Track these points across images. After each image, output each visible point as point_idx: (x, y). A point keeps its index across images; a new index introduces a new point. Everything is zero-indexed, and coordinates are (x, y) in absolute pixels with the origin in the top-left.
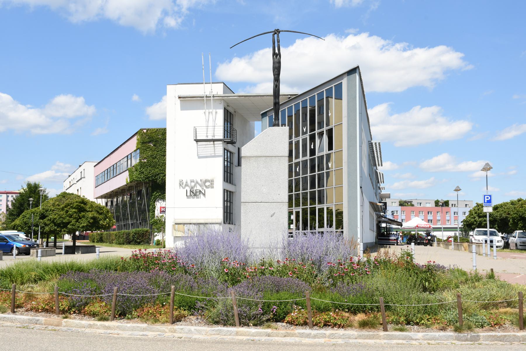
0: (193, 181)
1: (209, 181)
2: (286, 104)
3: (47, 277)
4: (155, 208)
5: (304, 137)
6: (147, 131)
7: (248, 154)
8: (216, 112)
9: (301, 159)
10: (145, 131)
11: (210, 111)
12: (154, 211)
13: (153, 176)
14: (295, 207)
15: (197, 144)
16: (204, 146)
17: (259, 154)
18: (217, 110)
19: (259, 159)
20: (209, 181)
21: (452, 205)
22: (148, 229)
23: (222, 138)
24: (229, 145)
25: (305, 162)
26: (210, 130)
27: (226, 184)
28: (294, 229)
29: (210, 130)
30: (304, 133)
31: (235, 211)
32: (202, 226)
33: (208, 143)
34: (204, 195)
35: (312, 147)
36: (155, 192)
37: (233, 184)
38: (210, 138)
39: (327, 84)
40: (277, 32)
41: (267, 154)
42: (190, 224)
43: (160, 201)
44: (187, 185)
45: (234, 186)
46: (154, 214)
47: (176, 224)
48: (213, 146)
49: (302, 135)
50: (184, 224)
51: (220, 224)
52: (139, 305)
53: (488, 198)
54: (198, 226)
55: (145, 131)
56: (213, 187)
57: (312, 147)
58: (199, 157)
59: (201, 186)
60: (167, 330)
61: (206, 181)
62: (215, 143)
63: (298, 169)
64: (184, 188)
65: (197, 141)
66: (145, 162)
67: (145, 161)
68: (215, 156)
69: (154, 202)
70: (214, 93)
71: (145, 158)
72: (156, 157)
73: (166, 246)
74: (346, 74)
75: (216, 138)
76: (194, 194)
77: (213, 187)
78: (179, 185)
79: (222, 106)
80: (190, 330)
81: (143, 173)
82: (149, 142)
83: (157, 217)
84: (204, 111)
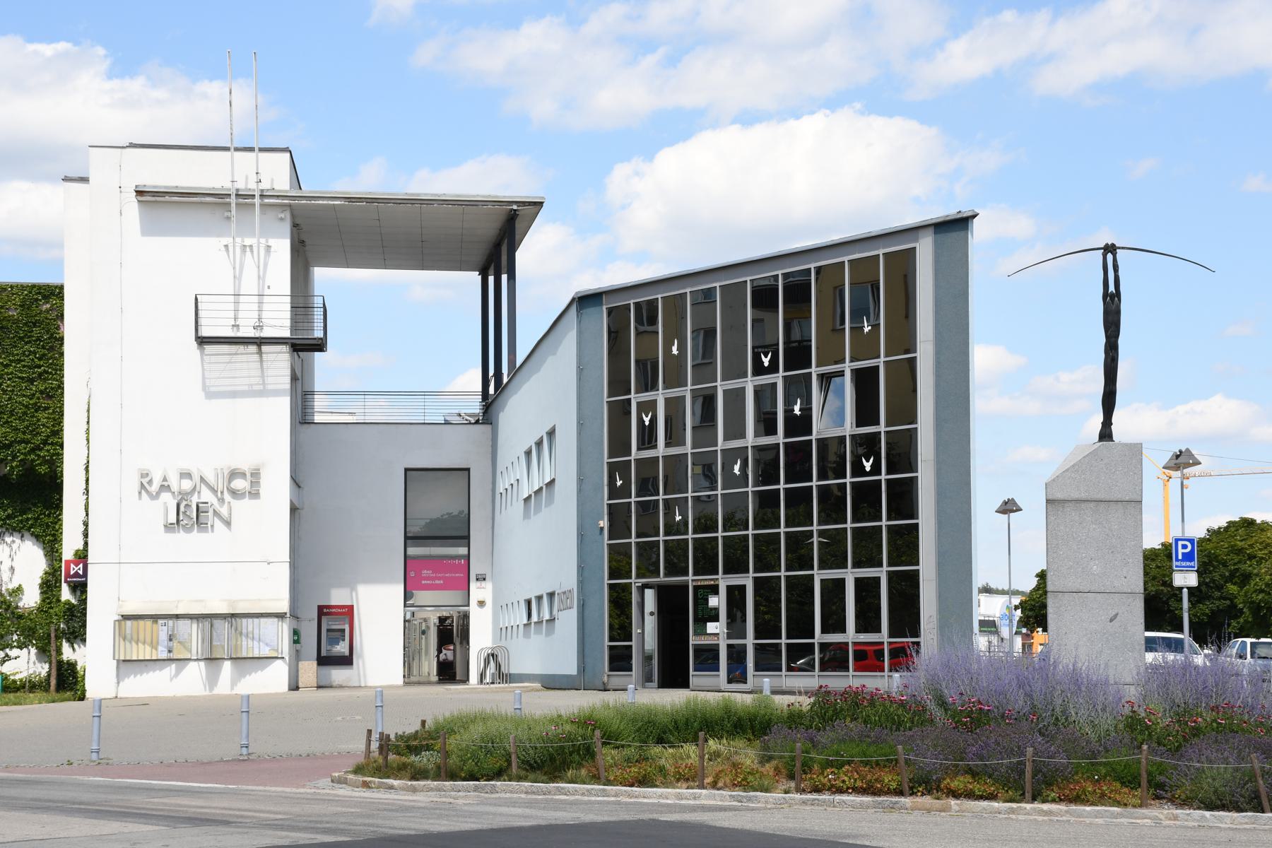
0: (186, 475)
1: (243, 475)
3: (607, 755)
14: (725, 572)
16: (226, 358)
17: (1083, 496)
18: (272, 242)
19: (1083, 505)
20: (243, 475)
23: (287, 334)
28: (723, 636)
32: (222, 627)
33: (241, 348)
34: (228, 523)
35: (797, 411)
39: (858, 245)
40: (1110, 249)
41: (1101, 496)
42: (177, 617)
43: (8, 539)
47: (126, 618)
48: (256, 357)
50: (155, 618)
51: (280, 616)
53: (1184, 547)
56: (255, 495)
57: (797, 411)
58: (210, 395)
59: (214, 491)
60: (1161, 816)
61: (234, 474)
62: (264, 348)
65: (202, 341)
68: (263, 393)
73: (88, 695)
74: (931, 230)
75: (267, 333)
76: (191, 517)
77: (255, 495)
78: (137, 487)
80: (1203, 817)
84: (225, 240)
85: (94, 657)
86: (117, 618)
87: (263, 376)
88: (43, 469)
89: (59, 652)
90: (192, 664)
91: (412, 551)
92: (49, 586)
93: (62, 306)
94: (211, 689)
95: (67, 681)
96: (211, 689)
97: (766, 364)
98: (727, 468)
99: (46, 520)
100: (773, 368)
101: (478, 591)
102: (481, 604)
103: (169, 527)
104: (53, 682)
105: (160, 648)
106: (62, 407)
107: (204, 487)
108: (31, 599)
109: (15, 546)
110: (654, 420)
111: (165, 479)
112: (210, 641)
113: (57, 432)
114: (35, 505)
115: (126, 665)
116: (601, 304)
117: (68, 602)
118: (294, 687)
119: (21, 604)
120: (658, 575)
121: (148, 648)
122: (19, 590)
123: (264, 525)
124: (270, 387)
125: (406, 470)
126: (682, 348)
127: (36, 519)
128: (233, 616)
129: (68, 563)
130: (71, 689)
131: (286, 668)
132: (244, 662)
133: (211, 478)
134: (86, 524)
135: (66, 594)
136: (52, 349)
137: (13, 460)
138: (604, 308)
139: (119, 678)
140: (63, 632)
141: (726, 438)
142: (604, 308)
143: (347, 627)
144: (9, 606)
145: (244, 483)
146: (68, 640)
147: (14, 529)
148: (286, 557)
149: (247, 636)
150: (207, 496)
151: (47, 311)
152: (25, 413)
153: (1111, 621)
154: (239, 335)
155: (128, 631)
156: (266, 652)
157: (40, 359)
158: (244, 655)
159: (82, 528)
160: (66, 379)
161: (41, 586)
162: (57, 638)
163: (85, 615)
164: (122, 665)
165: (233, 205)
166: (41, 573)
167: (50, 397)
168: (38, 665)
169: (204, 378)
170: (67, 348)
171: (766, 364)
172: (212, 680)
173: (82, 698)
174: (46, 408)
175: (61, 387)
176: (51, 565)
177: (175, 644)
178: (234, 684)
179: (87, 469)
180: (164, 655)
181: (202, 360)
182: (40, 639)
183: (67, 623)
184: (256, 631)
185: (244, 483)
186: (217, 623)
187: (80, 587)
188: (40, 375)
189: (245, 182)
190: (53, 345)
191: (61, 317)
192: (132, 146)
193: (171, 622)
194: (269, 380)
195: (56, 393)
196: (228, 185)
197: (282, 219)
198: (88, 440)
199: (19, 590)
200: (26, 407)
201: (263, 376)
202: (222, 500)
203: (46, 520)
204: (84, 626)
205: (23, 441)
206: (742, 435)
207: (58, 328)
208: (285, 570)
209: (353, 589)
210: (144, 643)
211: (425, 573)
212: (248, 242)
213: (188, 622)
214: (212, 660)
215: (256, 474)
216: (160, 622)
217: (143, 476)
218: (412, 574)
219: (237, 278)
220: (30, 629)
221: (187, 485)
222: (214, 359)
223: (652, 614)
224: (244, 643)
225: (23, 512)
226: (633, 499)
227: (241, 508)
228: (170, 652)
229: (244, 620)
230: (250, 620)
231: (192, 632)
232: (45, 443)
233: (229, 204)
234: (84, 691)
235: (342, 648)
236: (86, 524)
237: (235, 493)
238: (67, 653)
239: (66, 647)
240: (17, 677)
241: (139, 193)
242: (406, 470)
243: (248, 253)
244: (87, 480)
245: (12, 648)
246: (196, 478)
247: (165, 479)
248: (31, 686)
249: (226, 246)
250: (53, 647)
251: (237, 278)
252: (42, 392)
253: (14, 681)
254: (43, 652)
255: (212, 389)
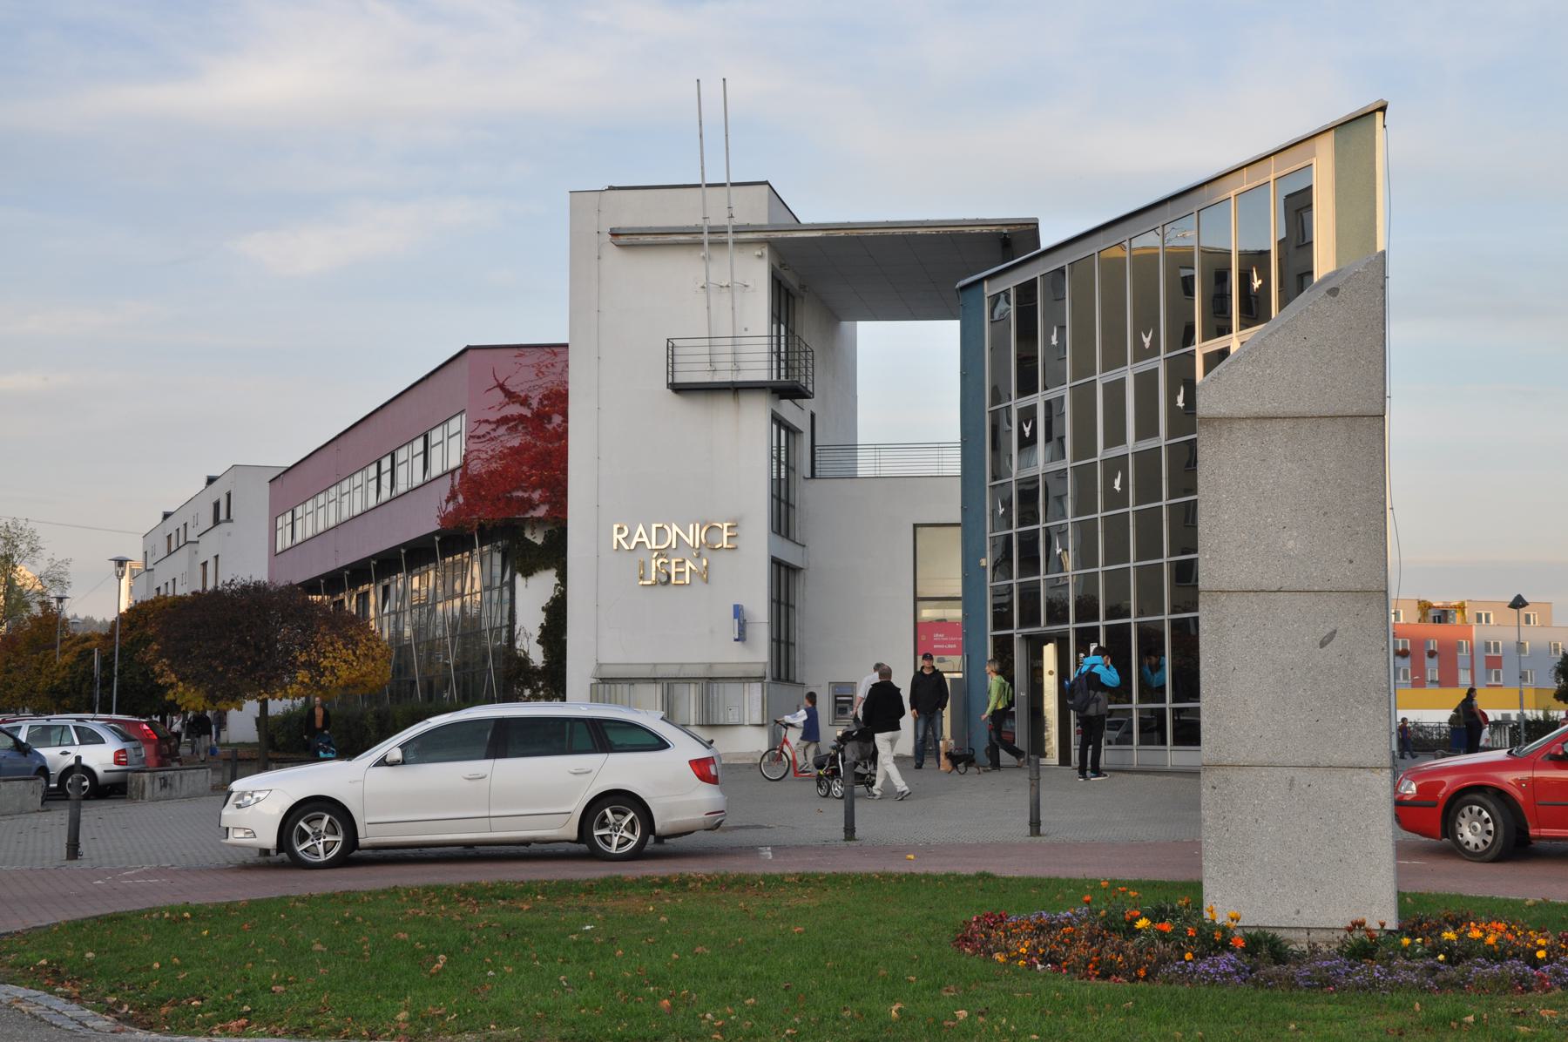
5: (1146, 366)
7: (1222, 409)
9: (1131, 445)
17: (1269, 408)
19: (1268, 424)
21: (1479, 617)
24: (786, 403)
25: (1148, 460)
27: (778, 539)
30: (1141, 354)
31: (798, 637)
37: (787, 536)
45: (800, 549)
47: (604, 680)
49: (1136, 360)
52: (83, 973)
63: (1117, 482)
65: (678, 389)
70: (740, 219)
97: (1147, 345)
98: (1108, 483)
100: (1154, 351)
110: (1034, 431)
120: (1038, 624)
125: (915, 526)
126: (1061, 337)
141: (1107, 446)
153: (1323, 644)
154: (716, 379)
171: (1147, 345)
189: (718, 218)
192: (611, 188)
196: (700, 222)
197: (760, 257)
206: (1123, 441)
211: (937, 636)
218: (923, 638)
223: (1051, 673)
242: (915, 526)
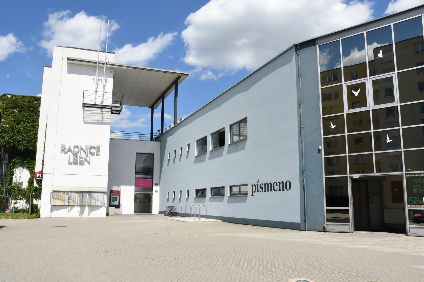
0: (77, 147)
1: (94, 148)
2: (365, 27)
4: (13, 174)
6: (12, 96)
8: (106, 80)
10: (9, 96)
11: (100, 78)
12: (12, 178)
13: (15, 142)
15: (84, 109)
16: (91, 112)
20: (94, 148)
22: (4, 196)
26: (100, 95)
29: (100, 95)
33: (96, 109)
36: (15, 159)
38: (98, 103)
42: (71, 192)
43: (19, 168)
44: (69, 150)
46: (11, 181)
47: (54, 191)
48: (101, 112)
50: (64, 192)
51: (105, 193)
54: (81, 195)
55: (9, 96)
56: (98, 155)
58: (85, 123)
59: (85, 152)
61: (92, 148)
62: (103, 110)
64: (65, 154)
66: (7, 127)
67: (7, 126)
68: (102, 123)
69: (13, 169)
71: (7, 123)
72: (20, 123)
73: (41, 216)
76: (77, 161)
77: (98, 155)
79: (112, 75)
81: (3, 137)
82: (14, 108)
83: (15, 183)
84: (93, 77)
85: (44, 204)
86: (52, 191)
87: (102, 118)
88: (31, 148)
89: (32, 201)
90: (76, 207)
91: (137, 176)
92: (30, 182)
93: (40, 102)
94: (81, 216)
95: (34, 211)
96: (81, 216)
99: (31, 163)
101: (155, 188)
102: (156, 191)
103: (70, 164)
104: (30, 211)
105: (65, 202)
106: (38, 131)
107: (82, 151)
108: (25, 185)
109: (21, 170)
111: (70, 148)
112: (82, 200)
113: (36, 138)
114: (28, 159)
115: (54, 207)
116: (316, 44)
117: (36, 187)
118: (108, 215)
119: (22, 187)
121: (61, 202)
122: (22, 183)
123: (101, 164)
124: (104, 122)
127: (28, 163)
128: (89, 192)
129: (37, 173)
130: (36, 213)
131: (106, 209)
132: (93, 208)
133: (84, 148)
134: (43, 161)
135: (35, 184)
136: (36, 114)
137: (22, 145)
138: (318, 46)
139: (52, 211)
140: (34, 195)
142: (318, 46)
143: (118, 197)
144: (18, 187)
145: (94, 150)
146: (35, 198)
147: (21, 165)
148: (106, 173)
149: (94, 199)
150: (83, 154)
151: (36, 104)
152: (27, 132)
155: (55, 196)
156: (100, 204)
157: (32, 117)
158: (93, 205)
159: (42, 162)
160: (39, 123)
161: (28, 182)
162: (32, 197)
163: (41, 190)
164: (53, 207)
165: (97, 67)
166: (28, 178)
167: (35, 128)
168: (26, 205)
169: (84, 118)
170: (41, 114)
172: (82, 213)
173: (39, 217)
174: (33, 131)
175: (38, 125)
176: (31, 176)
177: (70, 201)
178: (89, 214)
179: (44, 144)
180: (66, 204)
181: (84, 112)
182: (27, 197)
183: (35, 193)
184: (97, 198)
185: (94, 150)
186: (84, 194)
187: (40, 182)
188: (32, 121)
190: (37, 113)
191: (40, 106)
193: (69, 194)
194: (104, 120)
195: (36, 127)
197: (111, 72)
198: (45, 135)
199: (22, 183)
200: (27, 130)
201: (102, 118)
202: (87, 156)
203: (31, 163)
204: (41, 194)
205: (25, 140)
207: (39, 109)
208: (106, 178)
209: (119, 186)
210: (60, 200)
211: (140, 182)
212: (100, 78)
213: (75, 194)
214: (82, 206)
215: (99, 148)
216: (66, 193)
217: (62, 146)
219: (97, 88)
220: (24, 194)
221: (76, 150)
222: (87, 112)
224: (93, 201)
225: (24, 161)
226: (346, 134)
227: (93, 159)
228: (69, 203)
229: (93, 194)
230: (95, 194)
231: (76, 197)
232: (32, 140)
233: (96, 67)
234: (40, 215)
235: (116, 203)
236: (43, 161)
237: (92, 154)
238: (35, 202)
239: (34, 200)
240: (20, 208)
241: (68, 59)
243: (100, 81)
244: (44, 147)
245: (18, 200)
246: (80, 148)
247: (70, 148)
248: (24, 211)
249: (94, 79)
250: (30, 200)
251: (97, 88)
252: (32, 126)
253: (19, 209)
254: (28, 202)
255: (86, 121)
